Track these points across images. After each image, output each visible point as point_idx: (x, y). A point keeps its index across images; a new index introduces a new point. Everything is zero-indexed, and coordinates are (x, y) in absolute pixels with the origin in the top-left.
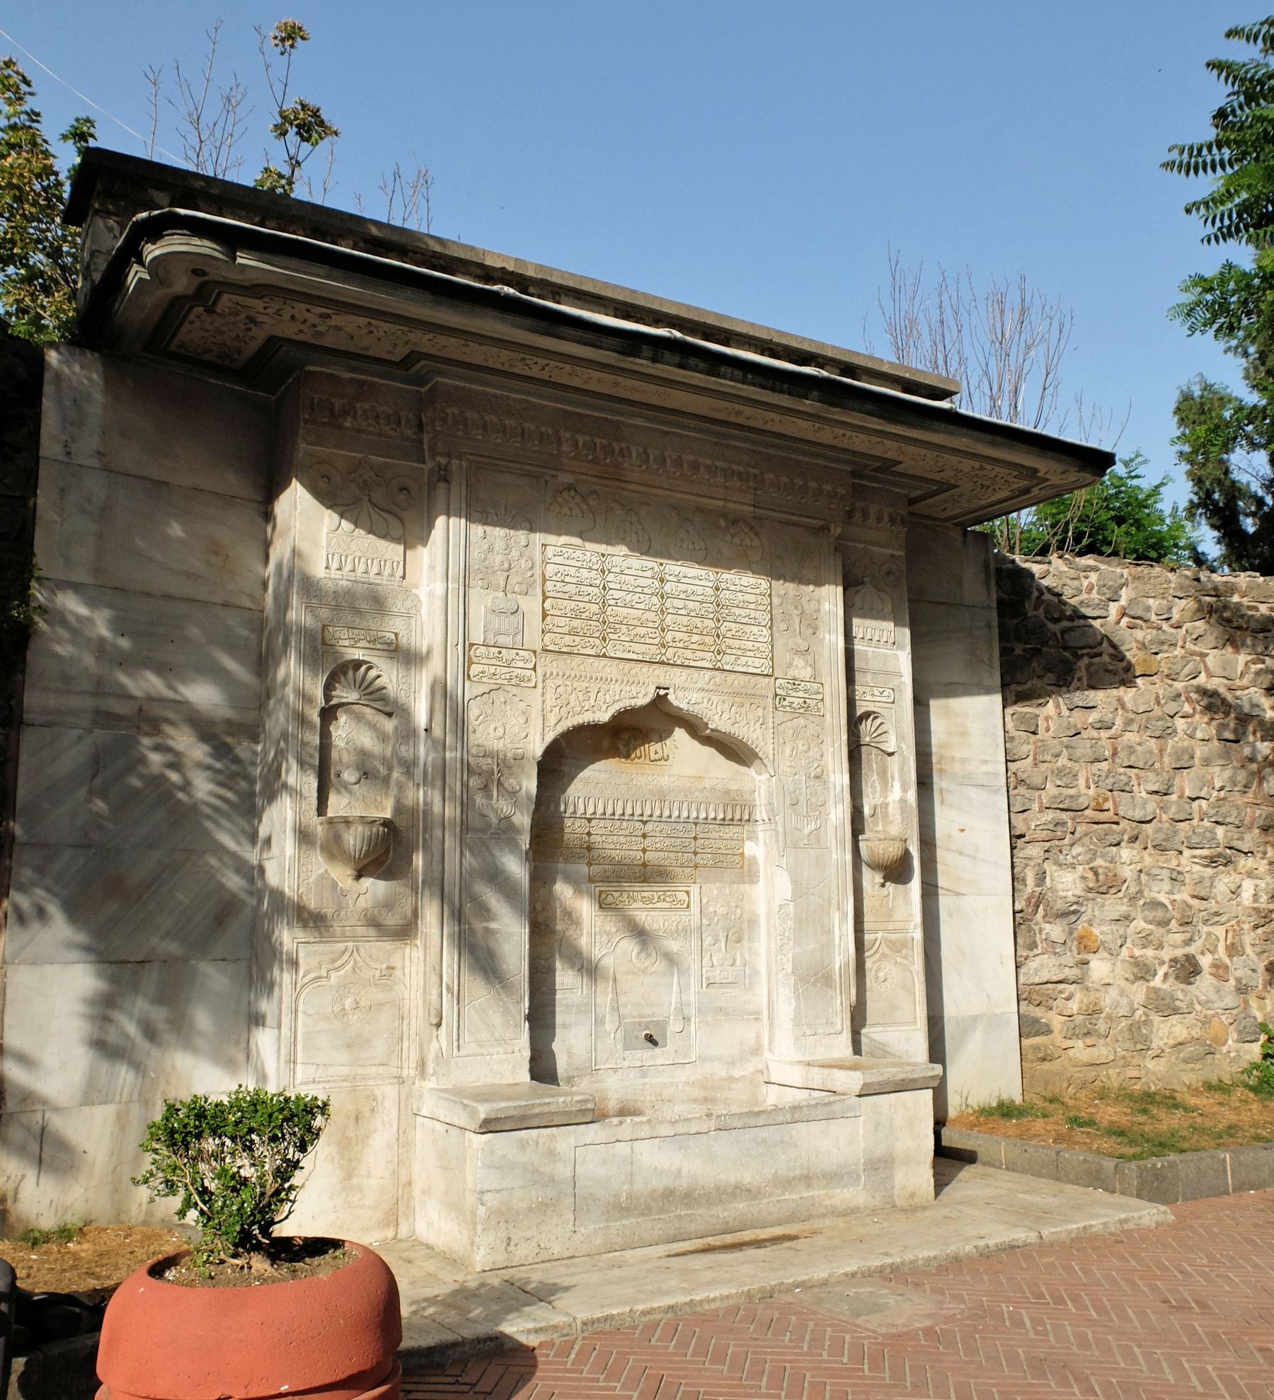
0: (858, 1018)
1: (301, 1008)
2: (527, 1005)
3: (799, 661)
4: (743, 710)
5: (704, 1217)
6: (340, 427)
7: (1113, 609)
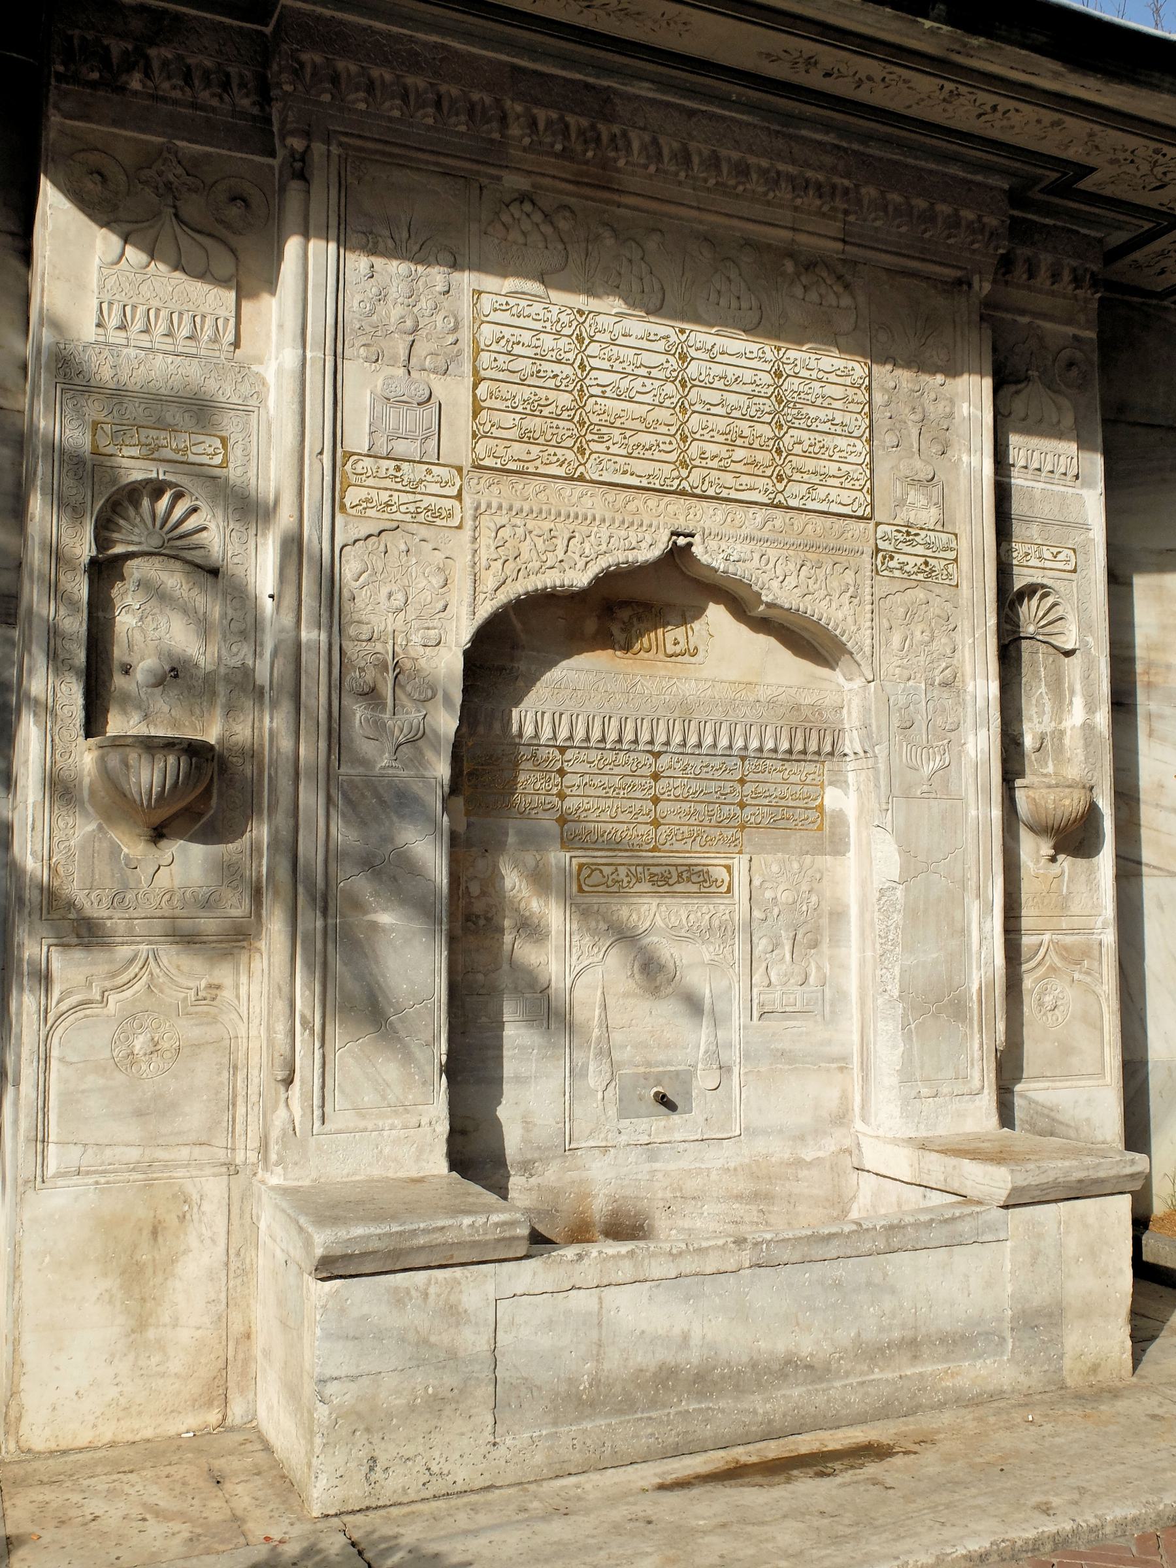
0: (1008, 1068)
1: (55, 1053)
2: (444, 1047)
3: (915, 496)
4: (821, 573)
5: (728, 1412)
6: (122, 89)
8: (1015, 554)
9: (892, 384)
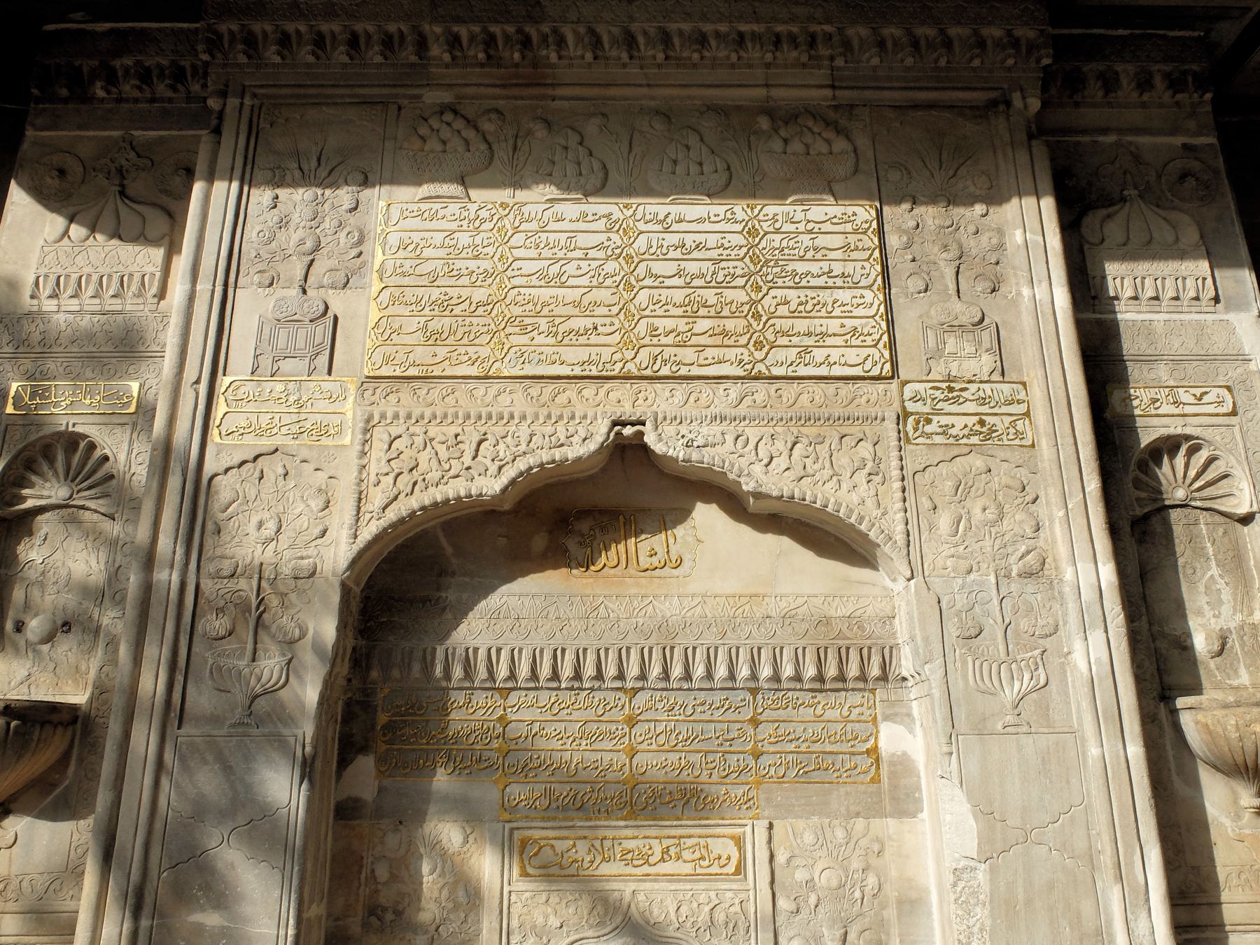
4: (823, 450)
8: (1135, 403)
9: (912, 224)
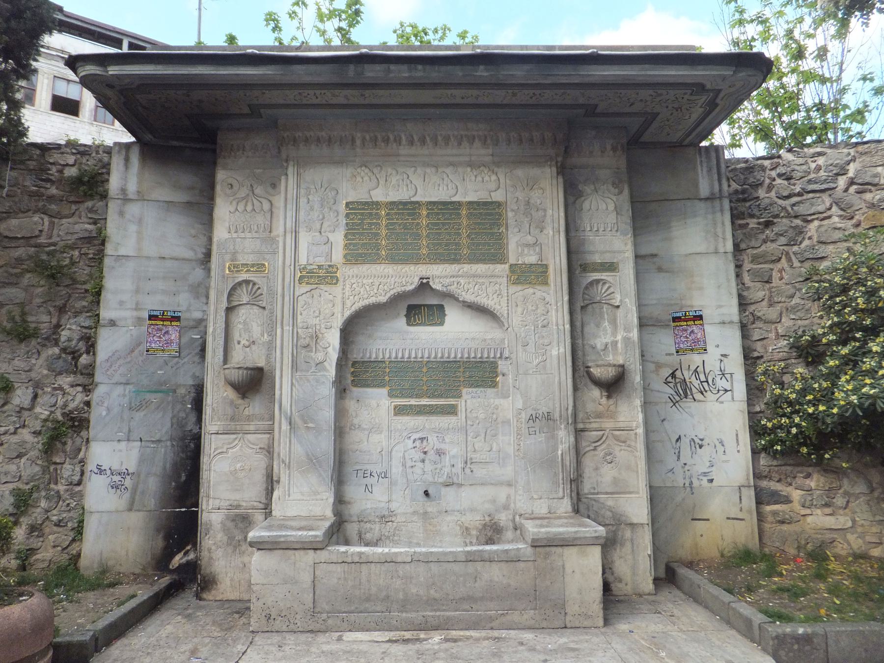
7: (842, 182)
